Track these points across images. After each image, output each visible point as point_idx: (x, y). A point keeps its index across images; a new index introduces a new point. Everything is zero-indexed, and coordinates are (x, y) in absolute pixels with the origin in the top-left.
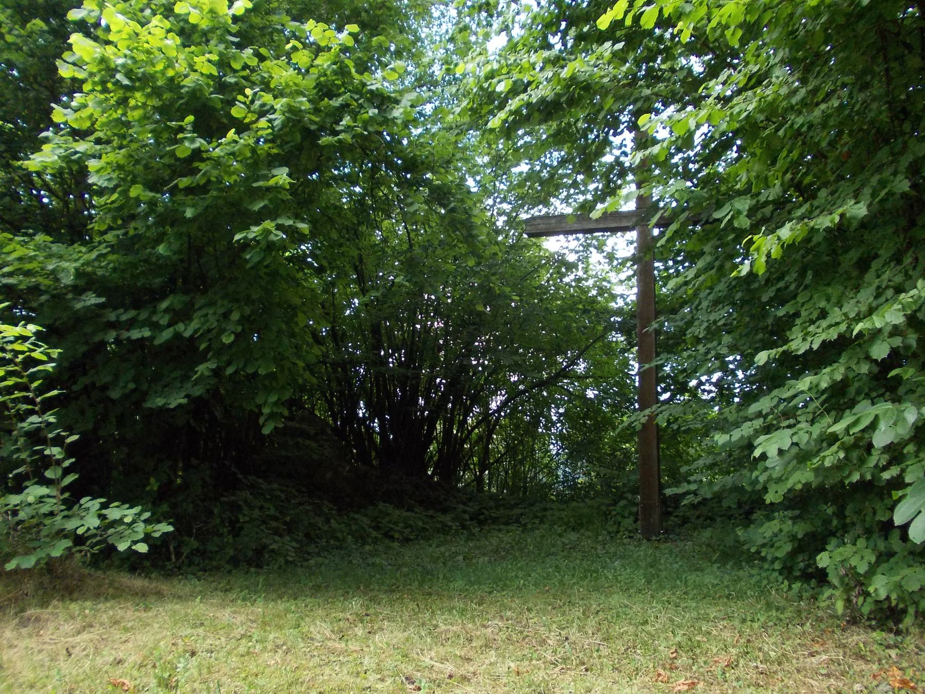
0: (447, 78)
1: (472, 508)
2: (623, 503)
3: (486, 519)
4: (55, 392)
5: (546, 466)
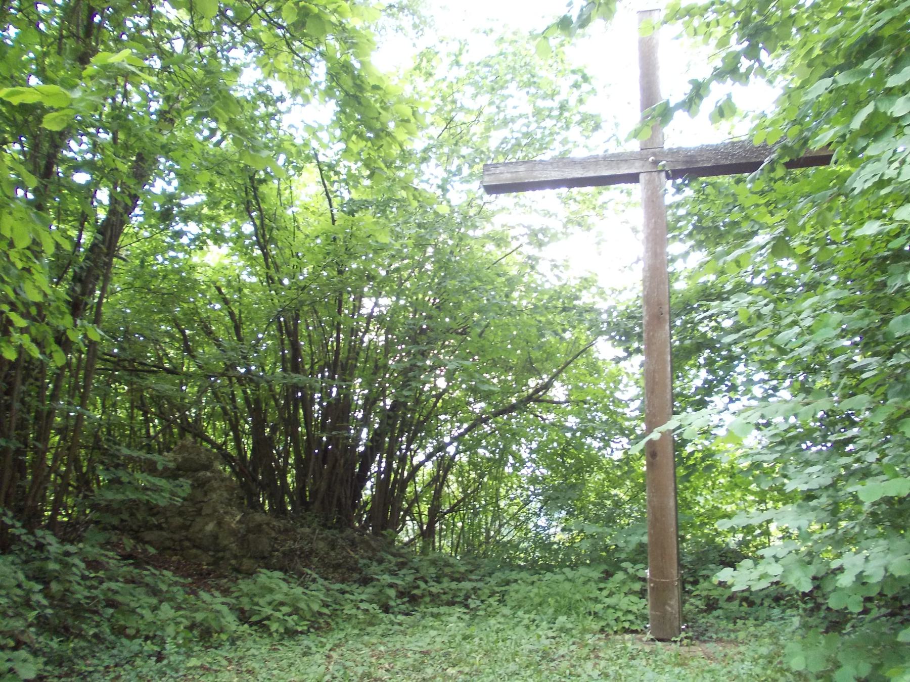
0: (608, 502)
1: (404, 579)
2: (620, 576)
3: (423, 596)
4: (358, 466)
5: (514, 516)
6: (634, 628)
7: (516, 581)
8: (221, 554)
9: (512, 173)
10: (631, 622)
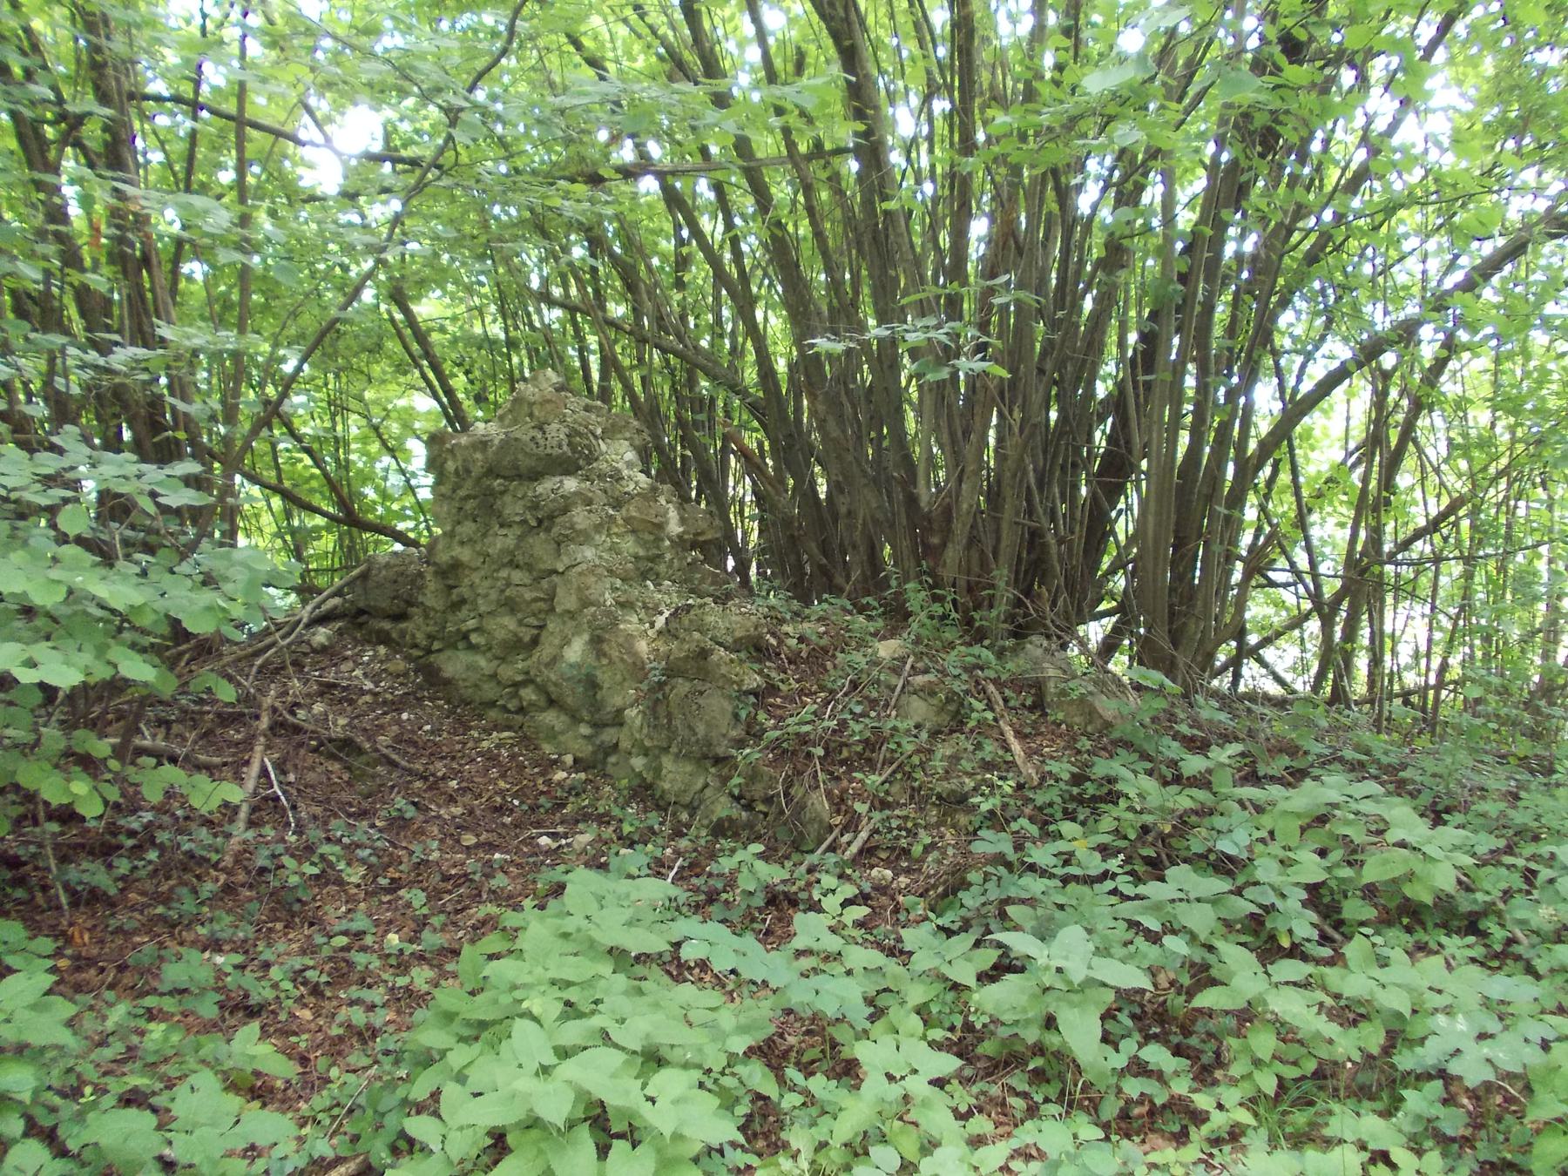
8: (609, 735)
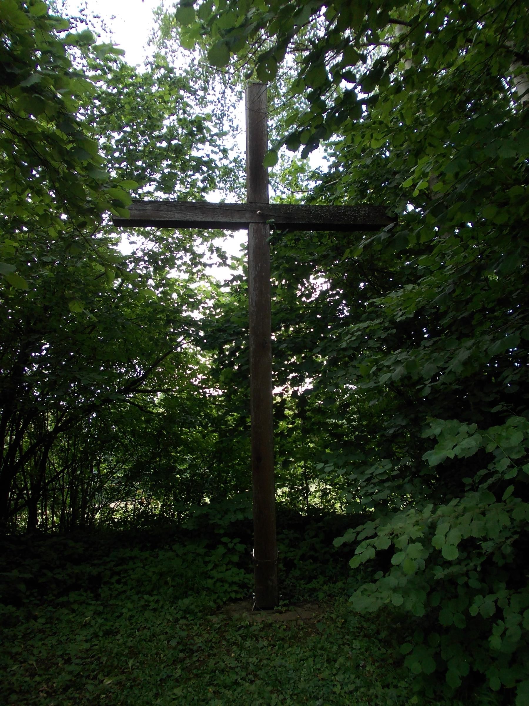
2: (221, 550)
6: (239, 596)
7: (131, 558)
9: (139, 210)
10: (236, 592)
